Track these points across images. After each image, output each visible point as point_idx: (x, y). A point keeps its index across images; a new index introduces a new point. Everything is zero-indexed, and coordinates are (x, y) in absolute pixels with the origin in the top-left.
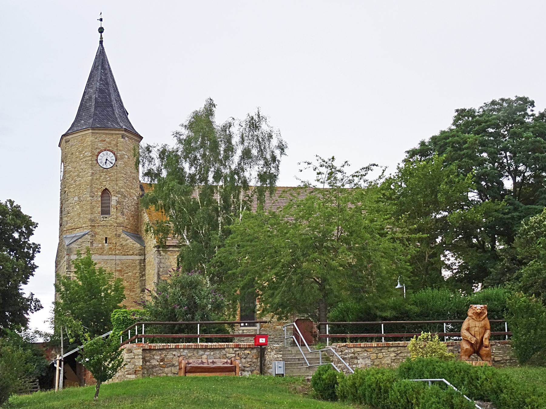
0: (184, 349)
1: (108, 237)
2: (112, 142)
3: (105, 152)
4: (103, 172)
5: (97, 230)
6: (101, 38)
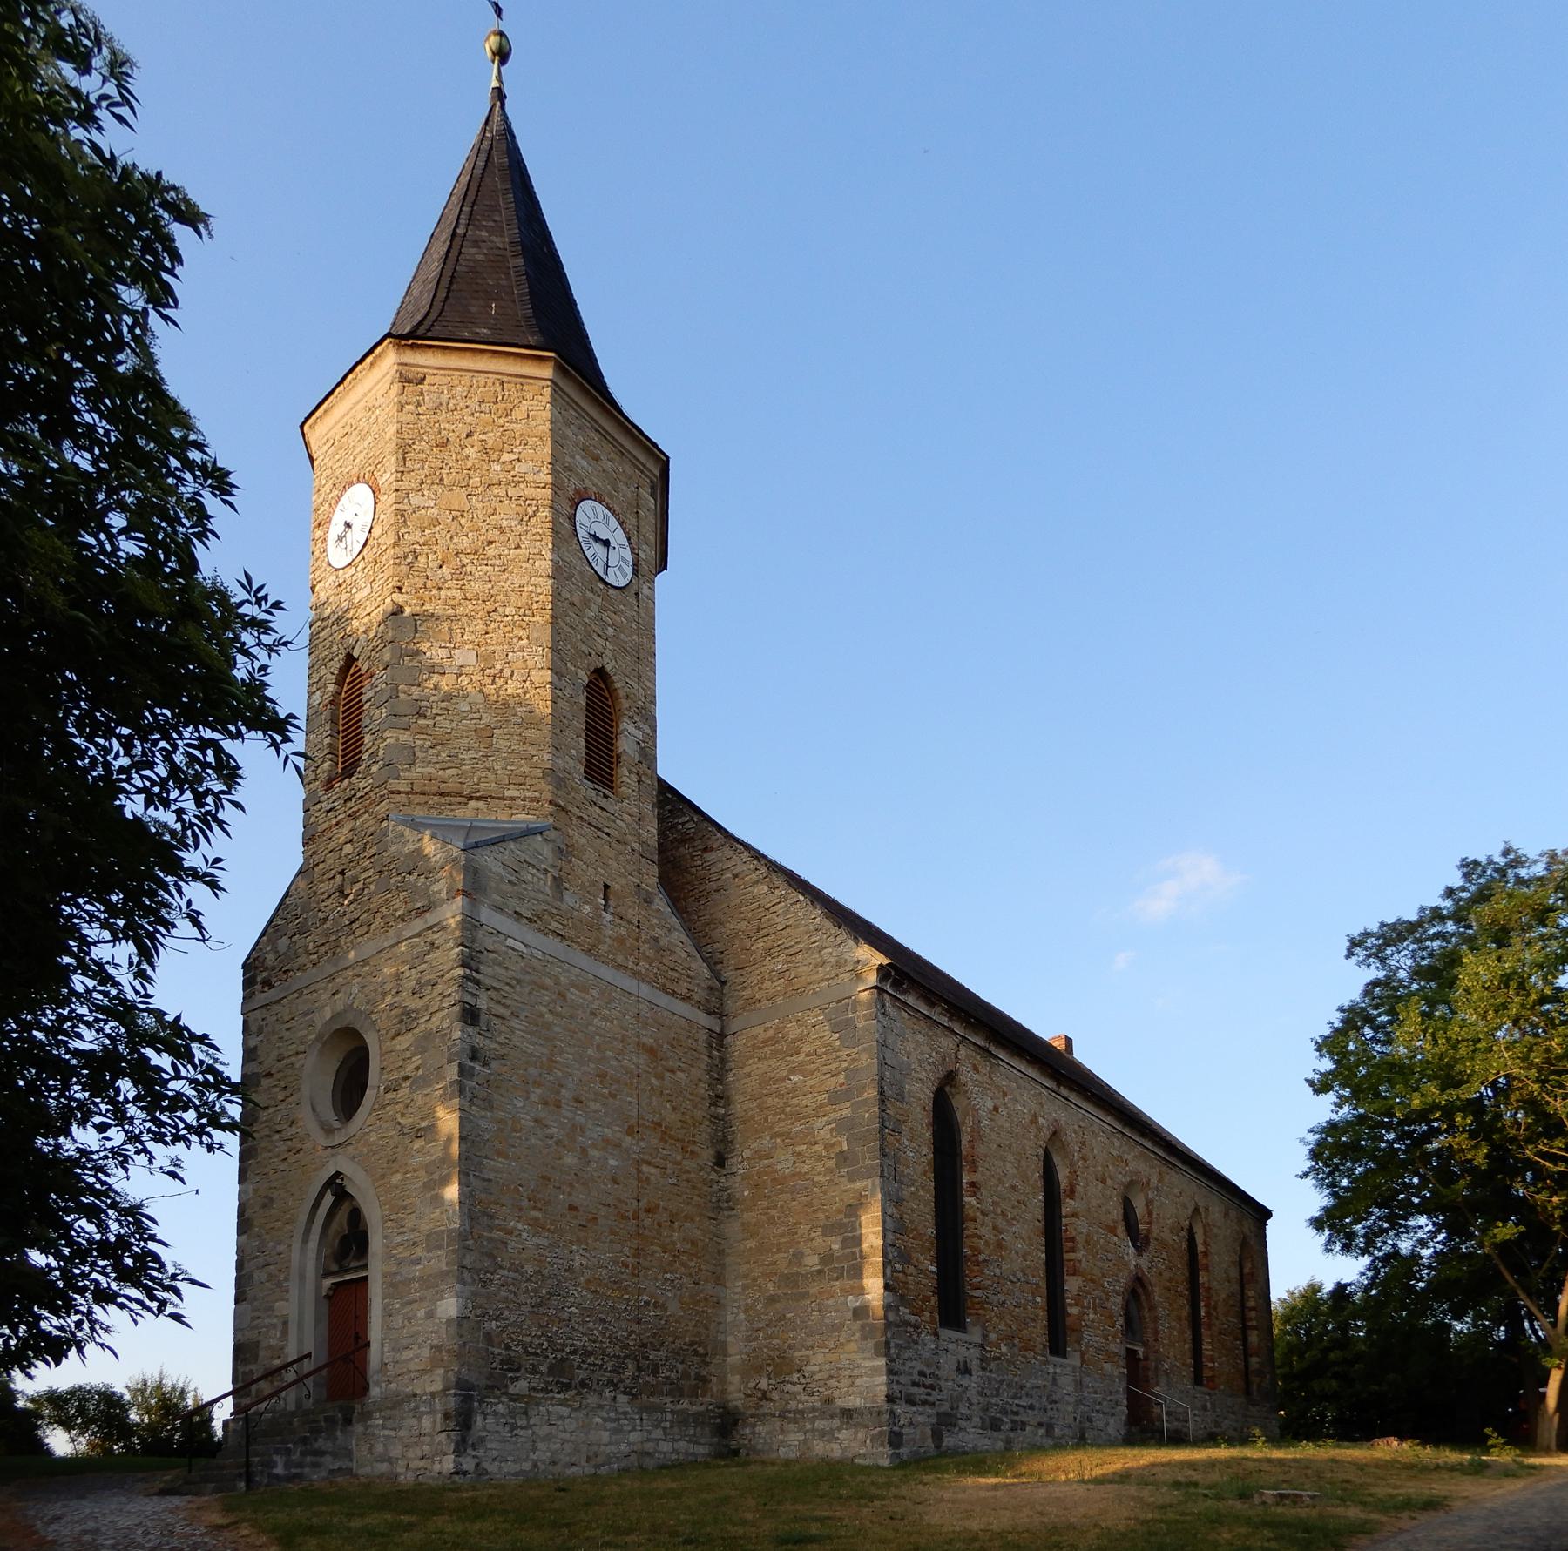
1: (615, 886)
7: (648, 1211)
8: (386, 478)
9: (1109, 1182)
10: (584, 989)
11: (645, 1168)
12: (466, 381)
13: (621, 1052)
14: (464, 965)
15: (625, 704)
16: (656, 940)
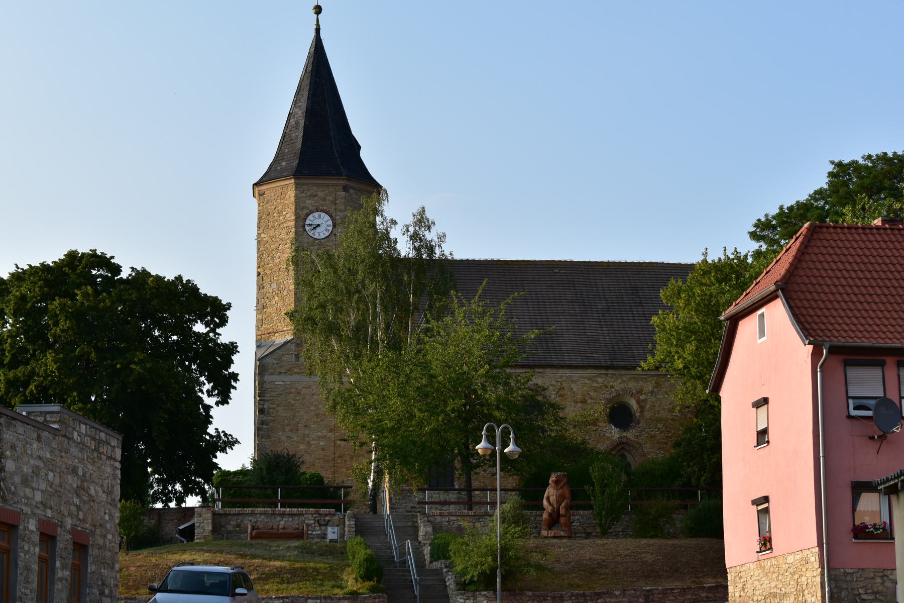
0: (261, 514)
2: (328, 198)
3: (316, 214)
4: (313, 245)
6: (318, 24)
9: (589, 401)
10: (309, 387)
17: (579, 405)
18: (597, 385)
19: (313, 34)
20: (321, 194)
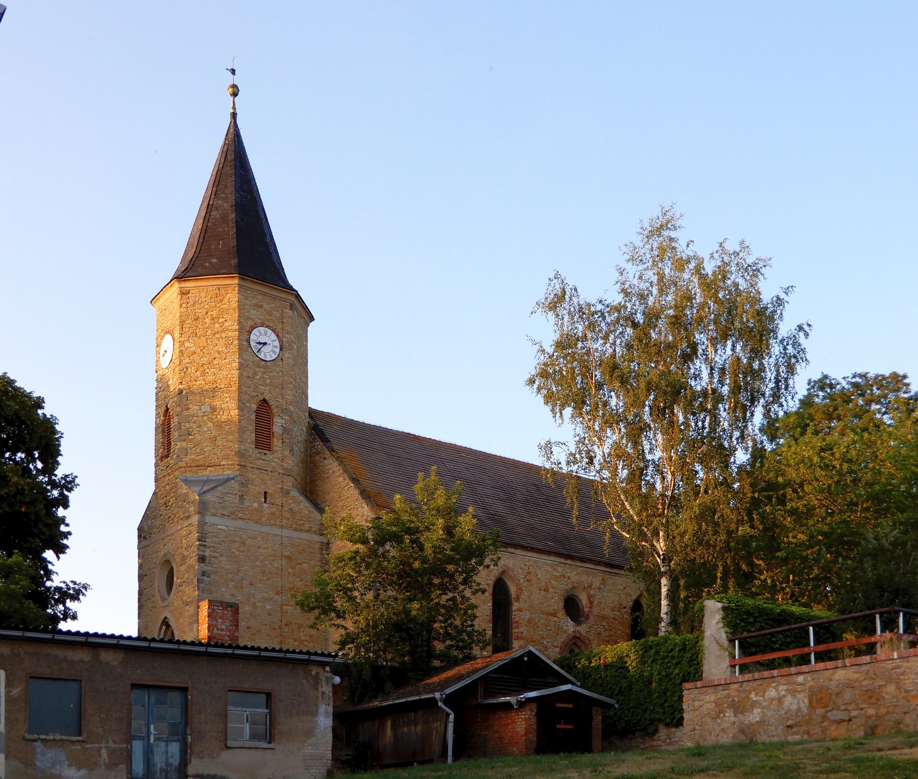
1: (270, 491)
4: (259, 367)
5: (251, 476)
7: (286, 625)
8: (177, 335)
9: (551, 590)
10: (255, 538)
11: (285, 607)
12: (205, 290)
13: (273, 561)
14: (199, 540)
15: (275, 410)
16: (291, 509)
17: (543, 593)
18: (557, 574)
19: (228, 120)
20: (266, 307)
